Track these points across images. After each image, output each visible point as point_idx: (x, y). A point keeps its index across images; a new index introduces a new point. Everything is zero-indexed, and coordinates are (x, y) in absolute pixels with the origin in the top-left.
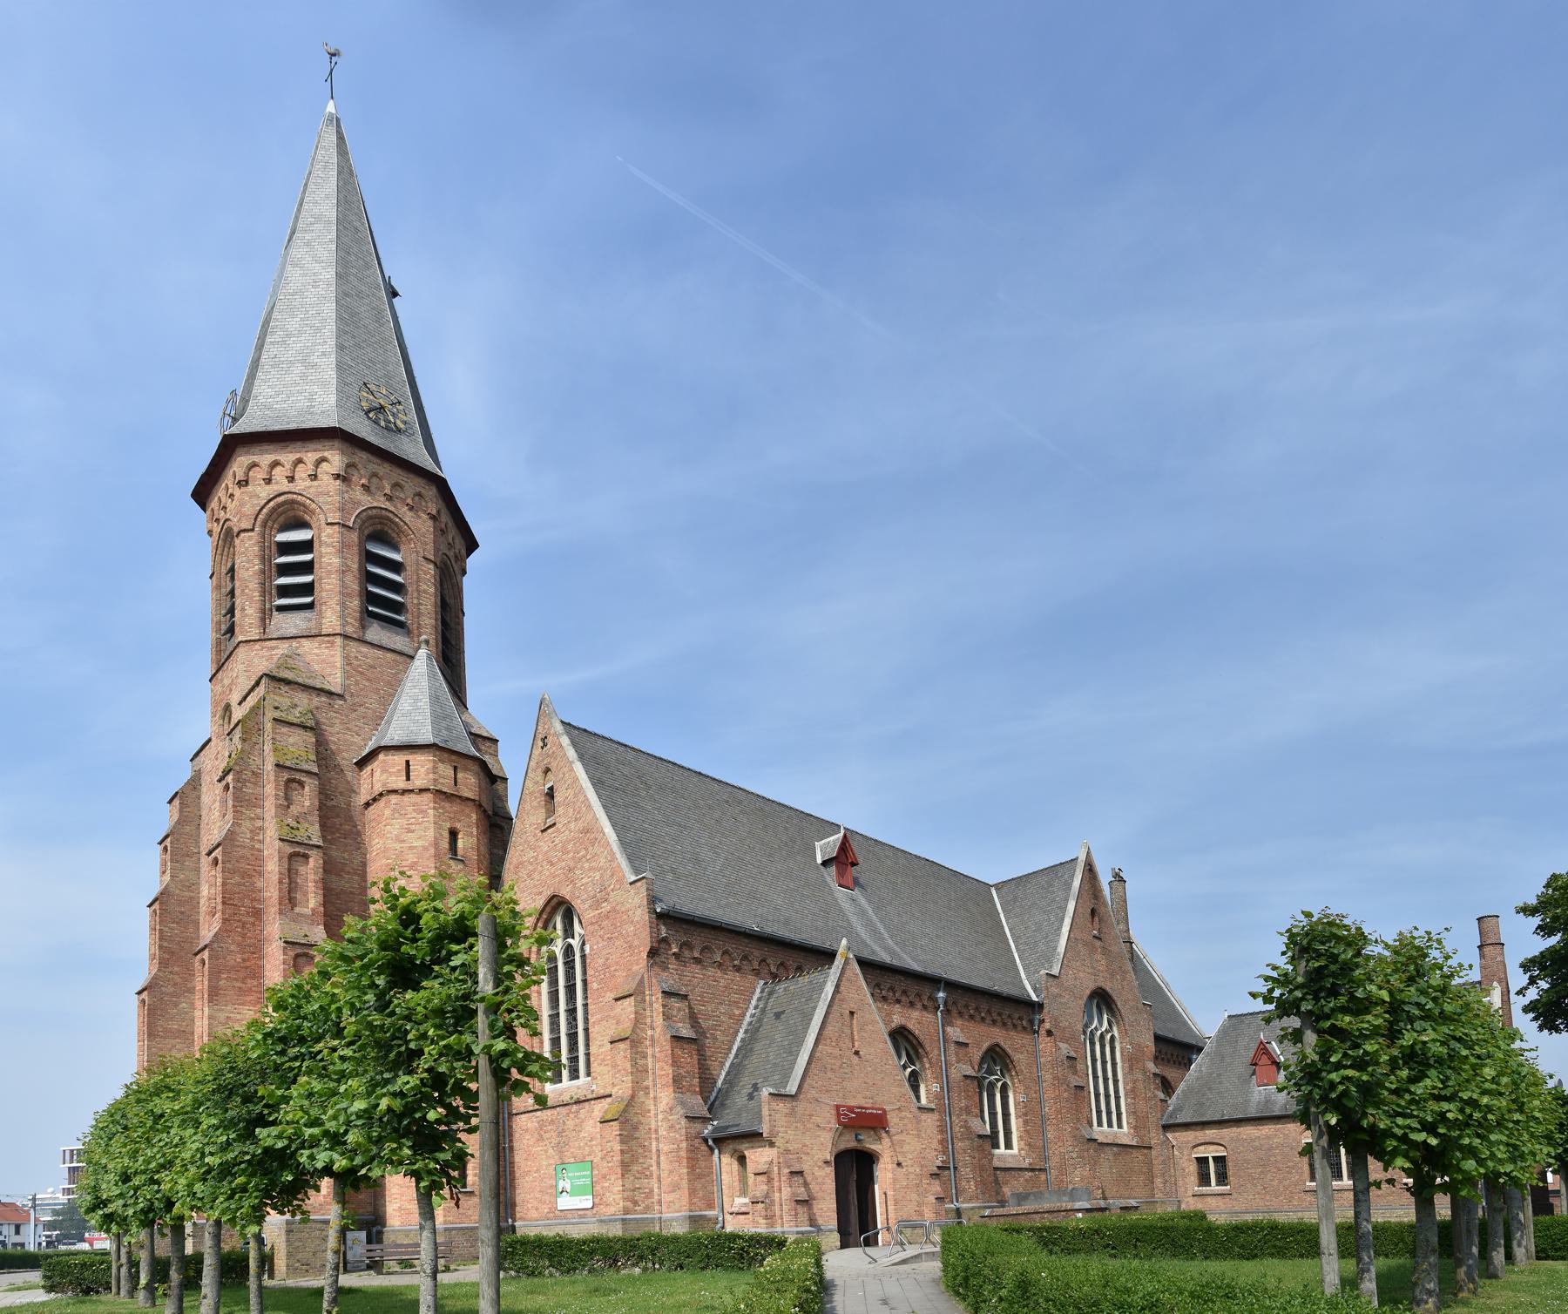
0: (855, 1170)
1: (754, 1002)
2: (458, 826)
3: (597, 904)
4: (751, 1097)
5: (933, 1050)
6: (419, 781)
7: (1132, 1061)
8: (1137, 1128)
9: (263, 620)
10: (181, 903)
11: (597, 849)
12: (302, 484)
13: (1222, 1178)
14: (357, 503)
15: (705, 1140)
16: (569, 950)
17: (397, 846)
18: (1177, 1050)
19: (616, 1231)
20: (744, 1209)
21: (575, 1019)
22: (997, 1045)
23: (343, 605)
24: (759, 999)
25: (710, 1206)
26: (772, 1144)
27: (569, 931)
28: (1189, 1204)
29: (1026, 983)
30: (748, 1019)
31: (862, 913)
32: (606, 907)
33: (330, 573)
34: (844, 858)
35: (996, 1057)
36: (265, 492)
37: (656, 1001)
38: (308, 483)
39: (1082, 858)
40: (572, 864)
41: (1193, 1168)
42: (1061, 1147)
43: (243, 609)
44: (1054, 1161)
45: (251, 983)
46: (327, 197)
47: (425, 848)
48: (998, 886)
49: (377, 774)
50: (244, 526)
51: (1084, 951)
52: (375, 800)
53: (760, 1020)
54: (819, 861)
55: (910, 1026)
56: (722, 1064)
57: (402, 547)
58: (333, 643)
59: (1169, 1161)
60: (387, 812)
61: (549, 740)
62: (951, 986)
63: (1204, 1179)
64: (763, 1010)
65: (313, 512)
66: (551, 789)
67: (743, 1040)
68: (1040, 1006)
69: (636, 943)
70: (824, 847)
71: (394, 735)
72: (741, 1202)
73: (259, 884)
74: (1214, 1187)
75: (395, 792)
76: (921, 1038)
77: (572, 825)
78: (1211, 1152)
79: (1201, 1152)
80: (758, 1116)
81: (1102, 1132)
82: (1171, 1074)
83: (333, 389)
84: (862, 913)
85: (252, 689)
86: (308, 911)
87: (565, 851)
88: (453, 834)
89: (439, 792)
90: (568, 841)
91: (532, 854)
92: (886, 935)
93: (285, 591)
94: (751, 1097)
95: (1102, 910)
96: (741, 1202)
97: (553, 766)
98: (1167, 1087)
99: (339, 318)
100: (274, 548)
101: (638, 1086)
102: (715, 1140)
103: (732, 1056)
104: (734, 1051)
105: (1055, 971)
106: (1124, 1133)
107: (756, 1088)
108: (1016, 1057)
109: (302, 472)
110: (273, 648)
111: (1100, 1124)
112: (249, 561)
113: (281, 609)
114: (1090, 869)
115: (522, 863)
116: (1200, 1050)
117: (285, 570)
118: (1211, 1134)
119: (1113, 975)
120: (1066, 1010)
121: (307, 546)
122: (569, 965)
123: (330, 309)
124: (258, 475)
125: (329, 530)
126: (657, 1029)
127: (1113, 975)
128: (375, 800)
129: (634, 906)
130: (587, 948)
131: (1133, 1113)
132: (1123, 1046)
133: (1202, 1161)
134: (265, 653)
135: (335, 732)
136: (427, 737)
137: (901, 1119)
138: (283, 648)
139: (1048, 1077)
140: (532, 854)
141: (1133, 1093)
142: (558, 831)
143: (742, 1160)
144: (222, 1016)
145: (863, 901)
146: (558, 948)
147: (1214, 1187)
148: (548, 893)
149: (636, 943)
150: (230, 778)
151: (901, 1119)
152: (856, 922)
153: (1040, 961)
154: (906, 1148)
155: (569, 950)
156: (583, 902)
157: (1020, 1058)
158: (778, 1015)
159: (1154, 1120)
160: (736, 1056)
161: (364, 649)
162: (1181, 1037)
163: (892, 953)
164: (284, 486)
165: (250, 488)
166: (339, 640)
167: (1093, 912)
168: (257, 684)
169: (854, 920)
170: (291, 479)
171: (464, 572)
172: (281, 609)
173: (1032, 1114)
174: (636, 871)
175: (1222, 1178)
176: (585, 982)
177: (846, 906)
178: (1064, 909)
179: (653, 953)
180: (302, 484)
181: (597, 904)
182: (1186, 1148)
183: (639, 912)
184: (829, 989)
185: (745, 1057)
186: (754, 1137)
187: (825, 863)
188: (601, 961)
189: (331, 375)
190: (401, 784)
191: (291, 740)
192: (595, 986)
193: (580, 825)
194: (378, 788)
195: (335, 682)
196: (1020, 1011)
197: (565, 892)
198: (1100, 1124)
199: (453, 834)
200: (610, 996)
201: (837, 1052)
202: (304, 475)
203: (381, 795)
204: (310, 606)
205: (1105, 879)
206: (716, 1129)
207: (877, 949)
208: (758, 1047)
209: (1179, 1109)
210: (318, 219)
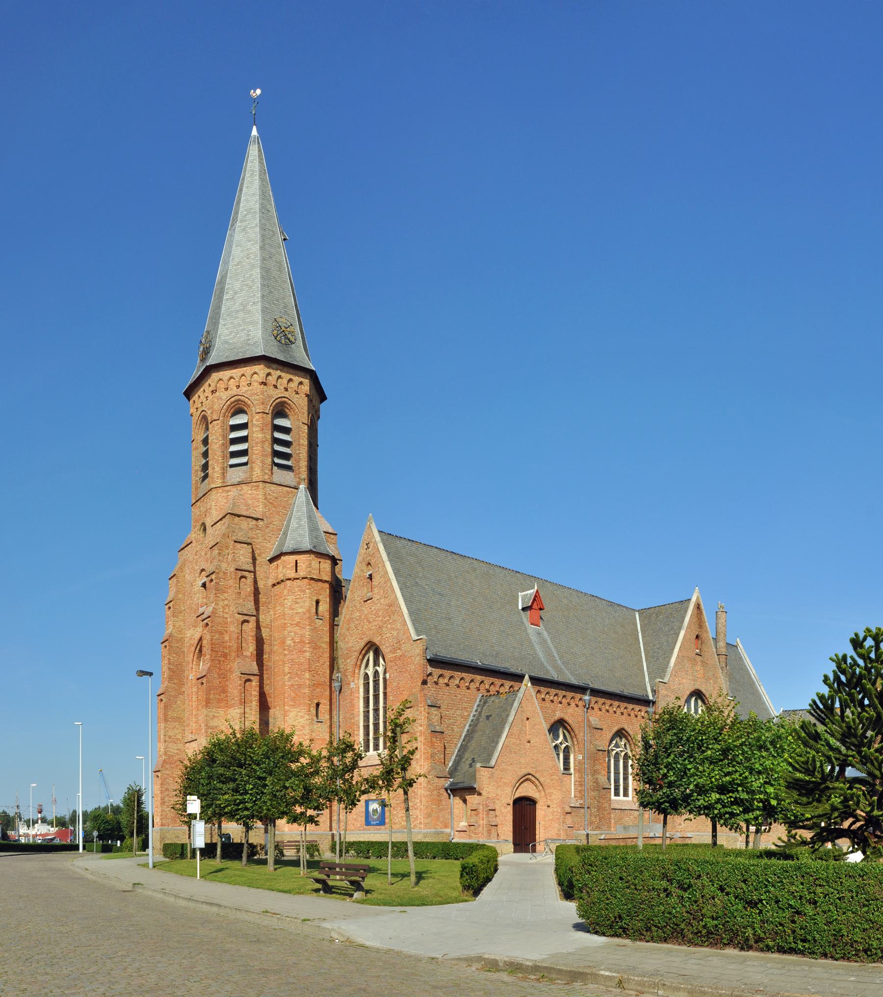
0: (524, 810)
1: (475, 708)
2: (320, 598)
3: (394, 651)
4: (471, 766)
5: (582, 734)
6: (301, 573)
9: (223, 474)
10: (178, 641)
11: (396, 617)
12: (244, 389)
14: (270, 397)
15: (446, 790)
16: (376, 673)
17: (290, 612)
20: (464, 829)
21: (378, 715)
22: (623, 729)
23: (263, 462)
24: (478, 706)
25: (446, 827)
26: (480, 794)
27: (376, 663)
29: (648, 685)
30: (471, 718)
31: (543, 642)
32: (399, 653)
33: (257, 443)
34: (535, 606)
38: (247, 388)
40: (381, 624)
43: (214, 468)
45: (223, 695)
46: (254, 194)
47: (304, 613)
48: (641, 612)
49: (280, 568)
50: (215, 417)
52: (278, 583)
53: (478, 719)
54: (520, 608)
55: (566, 718)
56: (456, 744)
57: (291, 417)
58: (258, 486)
60: (286, 592)
61: (371, 545)
64: (480, 713)
65: (249, 406)
66: (371, 575)
67: (468, 731)
68: (654, 703)
69: (415, 676)
70: (524, 597)
71: (289, 546)
75: (290, 579)
76: (573, 725)
77: (382, 601)
80: (474, 777)
83: (260, 326)
84: (543, 642)
85: (221, 520)
86: (248, 654)
88: (317, 602)
89: (312, 579)
90: (379, 610)
91: (358, 614)
92: (557, 658)
93: (234, 454)
94: (471, 766)
95: (704, 636)
97: (372, 562)
99: (262, 277)
100: (229, 428)
102: (451, 790)
103: (461, 740)
104: (463, 737)
105: (666, 680)
107: (473, 760)
110: (228, 491)
111: (617, 794)
112: (217, 439)
113: (232, 466)
115: (352, 619)
117: (234, 441)
119: (708, 679)
121: (244, 426)
122: (376, 682)
123: (257, 273)
125: (257, 417)
128: (278, 583)
130: (388, 675)
134: (224, 494)
135: (259, 543)
136: (307, 545)
137: (552, 780)
138: (233, 492)
140: (358, 614)
142: (373, 602)
143: (465, 801)
144: (211, 714)
145: (545, 634)
146: (370, 672)
148: (366, 640)
149: (415, 676)
150: (213, 576)
151: (552, 780)
152: (539, 647)
154: (553, 797)
155: (376, 673)
156: (387, 647)
158: (488, 717)
160: (464, 740)
161: (273, 487)
163: (559, 671)
164: (234, 391)
165: (217, 393)
166: (261, 484)
167: (697, 637)
168: (224, 517)
169: (537, 648)
170: (238, 387)
171: (319, 418)
172: (232, 466)
174: (418, 632)
176: (385, 694)
177: (534, 638)
178: (678, 635)
180: (244, 389)
181: (394, 651)
183: (418, 658)
185: (469, 741)
186: (472, 790)
187: (524, 609)
188: (395, 684)
190: (292, 574)
191: (241, 552)
192: (391, 698)
193: (387, 601)
194: (281, 577)
195: (259, 510)
197: (377, 640)
198: (617, 794)
199: (317, 602)
201: (518, 742)
202: (245, 384)
203: (282, 581)
204: (246, 464)
206: (452, 784)
207: (549, 668)
208: (476, 735)
210: (249, 211)
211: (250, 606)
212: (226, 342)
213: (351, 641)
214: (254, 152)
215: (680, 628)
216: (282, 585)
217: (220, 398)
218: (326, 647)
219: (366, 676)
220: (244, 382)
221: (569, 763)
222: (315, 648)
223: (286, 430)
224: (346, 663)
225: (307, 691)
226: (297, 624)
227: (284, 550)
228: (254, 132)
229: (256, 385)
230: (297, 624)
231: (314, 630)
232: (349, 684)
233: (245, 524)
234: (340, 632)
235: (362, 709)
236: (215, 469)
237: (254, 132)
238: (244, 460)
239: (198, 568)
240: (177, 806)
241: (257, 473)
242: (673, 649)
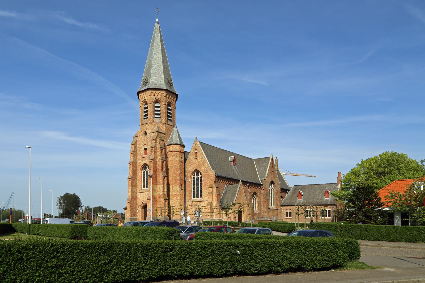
6: (178, 150)
7: (276, 194)
8: (276, 206)
13: (290, 216)
16: (198, 178)
18: (285, 190)
19: (210, 220)
28: (284, 220)
31: (236, 170)
32: (207, 173)
34: (234, 161)
35: (255, 194)
36: (154, 97)
37: (215, 189)
39: (271, 157)
41: (285, 214)
42: (264, 210)
44: (262, 212)
51: (270, 174)
59: (281, 212)
62: (250, 183)
63: (287, 216)
68: (262, 185)
70: (231, 158)
72: (225, 217)
73: (316, 241)
74: (289, 217)
78: (289, 211)
79: (287, 211)
81: (270, 206)
82: (283, 195)
87: (199, 163)
96: (225, 217)
97: (197, 149)
98: (282, 197)
101: (212, 200)
105: (265, 179)
106: (274, 207)
108: (258, 194)
109: (160, 95)
114: (272, 159)
116: (289, 190)
118: (289, 207)
119: (274, 178)
120: (266, 185)
121: (159, 107)
124: (153, 94)
126: (215, 192)
127: (274, 178)
129: (212, 174)
131: (276, 203)
132: (274, 190)
133: (287, 212)
139: (263, 197)
141: (276, 199)
146: (196, 178)
147: (289, 217)
153: (263, 176)
155: (198, 178)
157: (258, 194)
158: (229, 190)
159: (279, 205)
162: (286, 188)
164: (157, 97)
173: (259, 204)
175: (290, 216)
179: (215, 182)
180: (159, 97)
182: (285, 210)
184: (239, 188)
189: (163, 77)
190: (175, 150)
196: (259, 185)
197: (199, 169)
200: (208, 187)
205: (274, 158)
209: (284, 202)
211: (164, 158)
212: (153, 82)
213: (190, 169)
214: (157, 27)
215: (268, 165)
216: (172, 153)
217: (152, 98)
218: (183, 169)
219: (194, 178)
220: (160, 95)
221: (168, 70)
222: (181, 170)
223: (170, 110)
224: (188, 174)
225: (179, 181)
226: (176, 163)
227: (173, 143)
228: (157, 20)
229: (163, 96)
230: (176, 163)
231: (180, 165)
232: (189, 180)
233: (161, 135)
234: (187, 165)
235: (192, 187)
236: (150, 116)
237: (157, 20)
238: (159, 116)
239: (143, 144)
240: (403, 199)
241: (164, 121)
242: (266, 170)
